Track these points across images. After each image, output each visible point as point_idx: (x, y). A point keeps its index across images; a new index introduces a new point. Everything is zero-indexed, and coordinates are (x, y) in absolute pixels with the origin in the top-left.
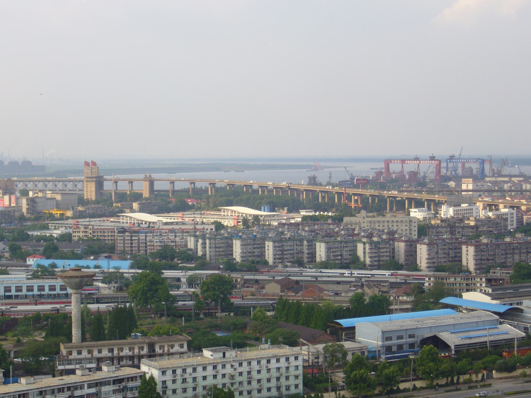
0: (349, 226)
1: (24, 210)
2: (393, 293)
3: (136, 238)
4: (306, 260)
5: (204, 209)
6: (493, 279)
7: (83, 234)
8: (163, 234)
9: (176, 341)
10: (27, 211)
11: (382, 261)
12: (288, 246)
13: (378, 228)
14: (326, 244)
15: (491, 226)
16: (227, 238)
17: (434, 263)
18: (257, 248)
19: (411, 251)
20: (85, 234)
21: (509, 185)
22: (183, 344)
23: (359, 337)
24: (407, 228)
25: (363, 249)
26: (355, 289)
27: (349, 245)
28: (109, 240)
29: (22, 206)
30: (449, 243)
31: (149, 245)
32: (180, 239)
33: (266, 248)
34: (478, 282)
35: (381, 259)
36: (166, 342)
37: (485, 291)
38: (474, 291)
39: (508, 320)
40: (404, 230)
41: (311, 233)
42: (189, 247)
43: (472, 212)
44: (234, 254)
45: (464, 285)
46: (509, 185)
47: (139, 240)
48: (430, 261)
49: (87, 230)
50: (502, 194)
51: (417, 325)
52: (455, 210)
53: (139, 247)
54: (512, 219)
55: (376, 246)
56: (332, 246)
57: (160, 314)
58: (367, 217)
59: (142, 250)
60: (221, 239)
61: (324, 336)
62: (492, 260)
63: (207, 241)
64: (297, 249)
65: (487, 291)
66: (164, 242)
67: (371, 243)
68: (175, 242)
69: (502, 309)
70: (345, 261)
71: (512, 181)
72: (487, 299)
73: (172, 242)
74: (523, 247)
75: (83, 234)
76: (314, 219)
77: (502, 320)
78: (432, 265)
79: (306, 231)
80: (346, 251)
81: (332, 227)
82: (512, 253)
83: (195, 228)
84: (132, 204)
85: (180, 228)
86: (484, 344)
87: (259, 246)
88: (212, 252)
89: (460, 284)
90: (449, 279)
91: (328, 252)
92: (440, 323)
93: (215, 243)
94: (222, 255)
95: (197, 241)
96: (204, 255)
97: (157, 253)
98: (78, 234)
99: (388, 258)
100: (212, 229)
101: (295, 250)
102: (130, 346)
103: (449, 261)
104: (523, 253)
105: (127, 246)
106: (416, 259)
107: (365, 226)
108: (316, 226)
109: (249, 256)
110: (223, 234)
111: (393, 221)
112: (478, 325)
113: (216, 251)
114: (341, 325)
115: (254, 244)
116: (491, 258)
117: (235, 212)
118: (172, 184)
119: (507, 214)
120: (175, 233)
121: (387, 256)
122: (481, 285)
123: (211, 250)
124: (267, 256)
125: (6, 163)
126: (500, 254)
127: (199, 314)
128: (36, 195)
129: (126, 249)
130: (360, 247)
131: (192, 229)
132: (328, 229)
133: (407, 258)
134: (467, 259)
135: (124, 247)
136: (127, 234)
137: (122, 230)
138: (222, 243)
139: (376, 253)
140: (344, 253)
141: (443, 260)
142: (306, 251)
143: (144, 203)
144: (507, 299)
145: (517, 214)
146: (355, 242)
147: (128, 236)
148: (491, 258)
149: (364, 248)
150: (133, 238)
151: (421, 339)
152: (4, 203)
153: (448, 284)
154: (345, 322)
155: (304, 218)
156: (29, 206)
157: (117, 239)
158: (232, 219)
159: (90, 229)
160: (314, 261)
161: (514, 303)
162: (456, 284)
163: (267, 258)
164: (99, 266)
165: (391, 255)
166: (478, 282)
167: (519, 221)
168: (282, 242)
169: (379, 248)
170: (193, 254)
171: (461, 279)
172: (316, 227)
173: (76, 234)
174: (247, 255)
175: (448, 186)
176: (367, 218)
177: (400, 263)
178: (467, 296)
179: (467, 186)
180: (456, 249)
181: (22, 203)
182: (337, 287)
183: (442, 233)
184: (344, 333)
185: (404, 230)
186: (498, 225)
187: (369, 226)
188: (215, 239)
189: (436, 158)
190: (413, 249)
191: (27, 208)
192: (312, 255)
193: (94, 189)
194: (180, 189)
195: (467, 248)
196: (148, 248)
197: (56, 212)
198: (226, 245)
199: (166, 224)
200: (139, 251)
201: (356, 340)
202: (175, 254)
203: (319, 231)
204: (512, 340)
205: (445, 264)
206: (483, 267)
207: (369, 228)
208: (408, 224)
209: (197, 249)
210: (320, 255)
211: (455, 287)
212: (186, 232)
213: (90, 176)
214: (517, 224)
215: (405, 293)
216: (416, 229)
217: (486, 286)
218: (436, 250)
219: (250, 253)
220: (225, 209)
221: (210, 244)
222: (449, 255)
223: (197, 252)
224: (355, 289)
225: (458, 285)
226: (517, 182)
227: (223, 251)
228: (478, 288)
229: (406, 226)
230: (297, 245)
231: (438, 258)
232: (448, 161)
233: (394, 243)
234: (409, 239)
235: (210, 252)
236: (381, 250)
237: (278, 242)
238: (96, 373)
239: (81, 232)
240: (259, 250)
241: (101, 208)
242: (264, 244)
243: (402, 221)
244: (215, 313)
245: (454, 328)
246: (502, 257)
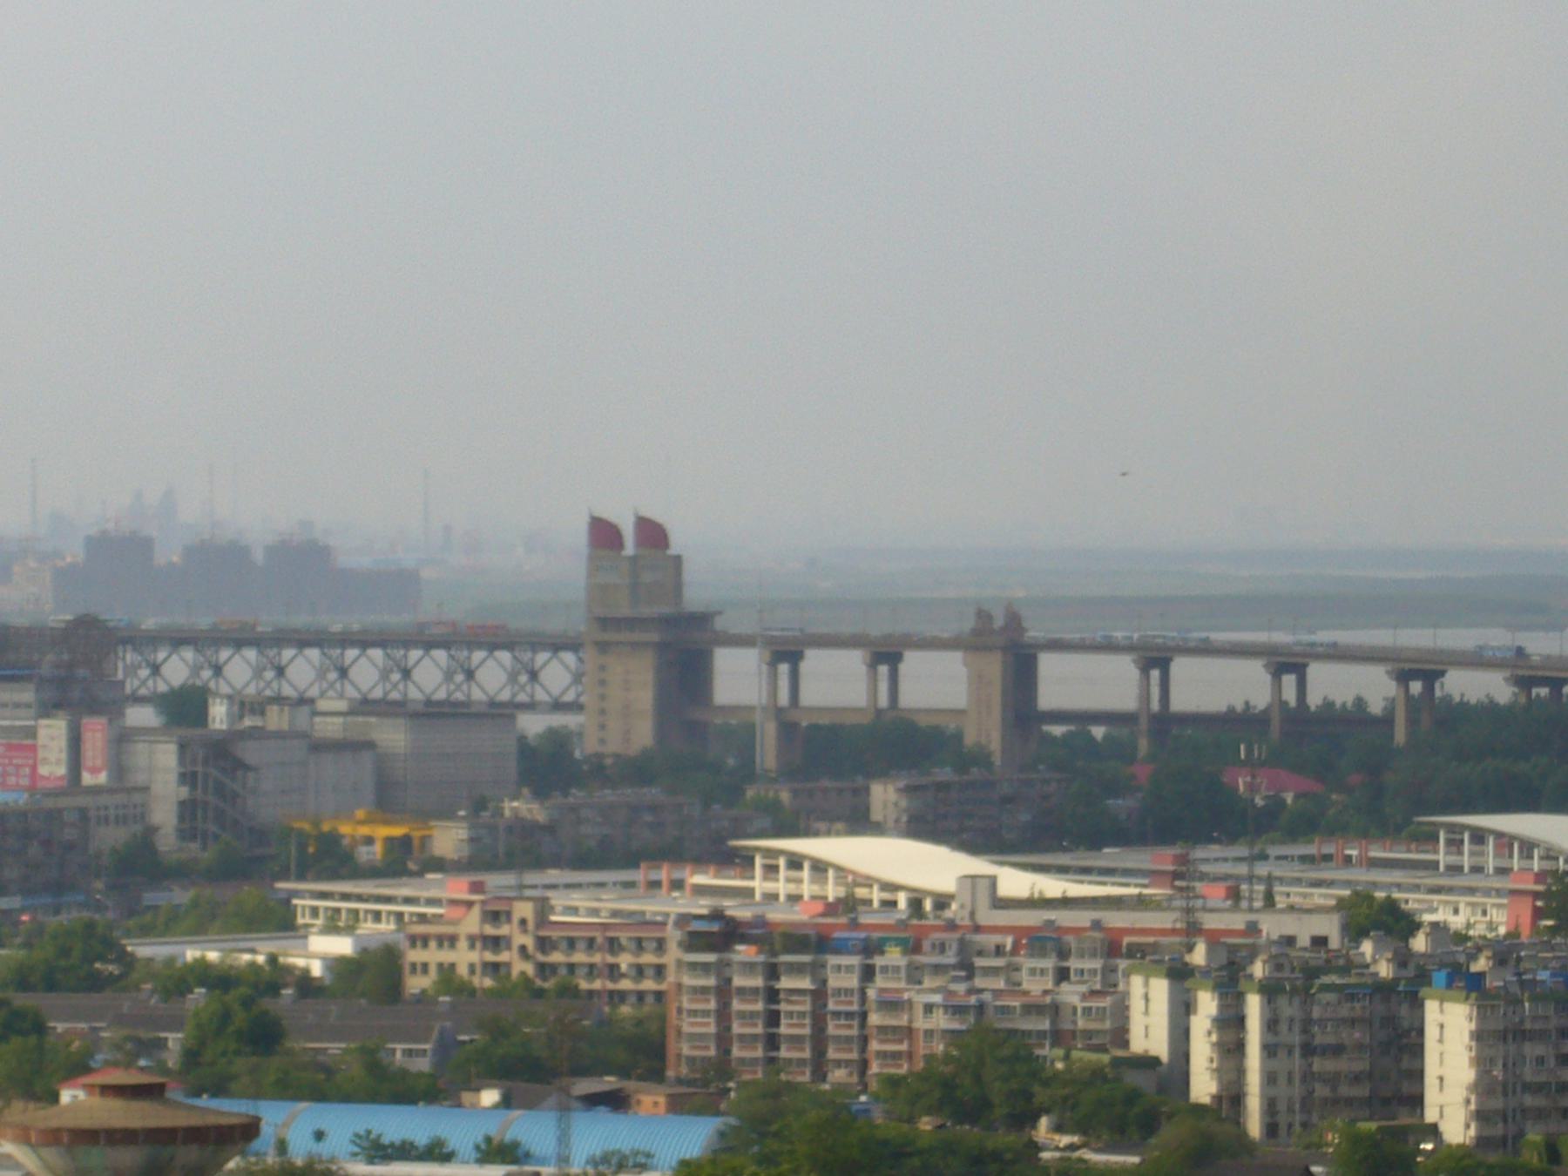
1: (164, 815)
3: (805, 983)
5: (1337, 830)
7: (475, 956)
8: (980, 962)
10: (181, 818)
16: (1384, 989)
20: (490, 957)
28: (641, 996)
29: (145, 789)
31: (882, 1029)
32: (1084, 997)
47: (819, 995)
49: (504, 930)
53: (819, 1040)
59: (838, 1063)
60: (1348, 994)
63: (1254, 1005)
68: (1055, 1010)
73: (1032, 1009)
75: (475, 956)
84: (867, 790)
88: (1282, 1080)
94: (1349, 1102)
97: (924, 1077)
98: (446, 956)
105: (742, 1037)
113: (1308, 1076)
118: (1155, 674)
120: (1063, 954)
125: (169, 553)
128: (248, 722)
129: (736, 1052)
131: (1174, 931)
135: (724, 1039)
136: (744, 952)
137: (715, 927)
138: (1352, 1022)
143: (942, 787)
147: (749, 967)
150: (785, 983)
152: (34, 768)
156: (193, 786)
157: (679, 986)
158: (1499, 892)
159: (523, 922)
164: (515, 1145)
173: (433, 955)
191: (182, 804)
193: (644, 698)
196: (874, 1046)
197: (364, 830)
200: (819, 1067)
202: (1036, 1088)
213: (625, 611)
219: (1537, 1088)
220: (1464, 827)
221: (1271, 1025)
227: (1356, 1079)
239: (463, 944)
241: (653, 808)
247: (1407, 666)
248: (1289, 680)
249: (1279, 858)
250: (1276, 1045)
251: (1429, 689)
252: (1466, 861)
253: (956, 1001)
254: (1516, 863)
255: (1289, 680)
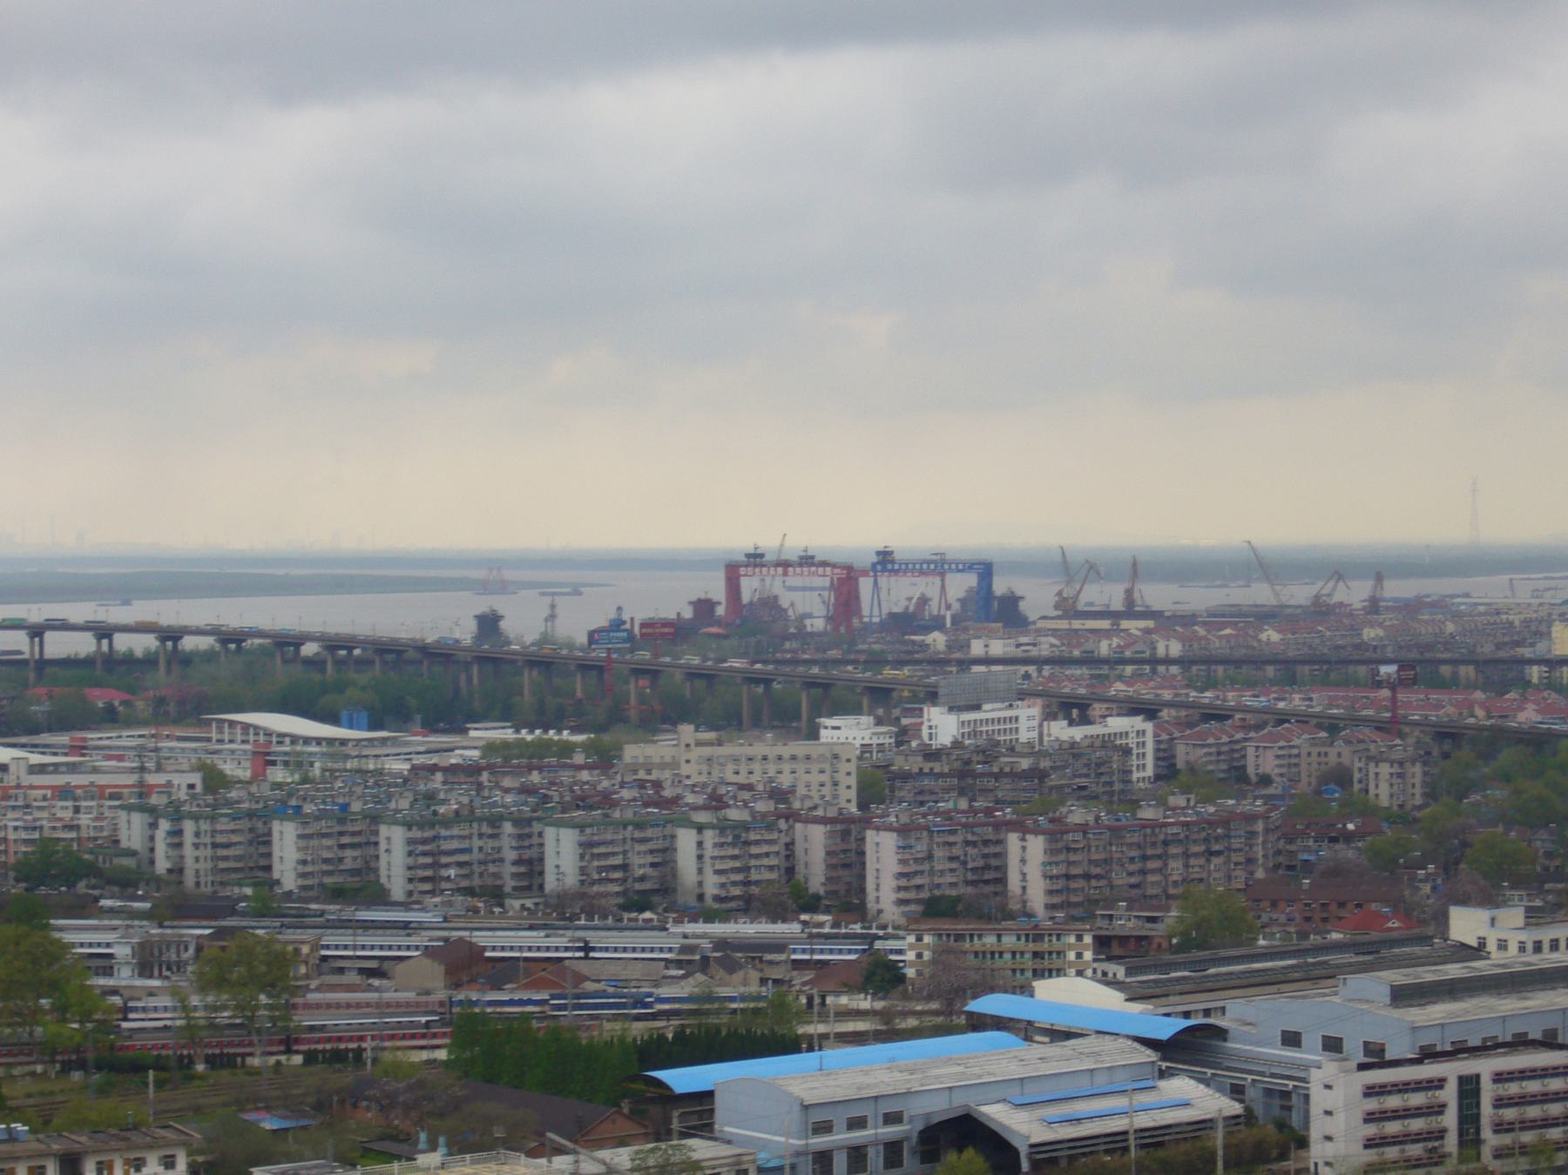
0: (642, 775)
2: (804, 984)
4: (509, 884)
6: (1115, 936)
9: (150, 1147)
11: (757, 883)
12: (452, 837)
13: (731, 778)
14: (577, 831)
15: (1080, 772)
16: (251, 815)
17: (919, 887)
18: (353, 846)
19: (845, 851)
21: (1115, 642)
22: (173, 1156)
23: (725, 1124)
24: (824, 778)
25: (694, 845)
26: (682, 972)
27: (649, 833)
30: (965, 826)
33: (383, 846)
34: (1070, 947)
35: (754, 876)
36: (118, 1150)
37: (1105, 974)
38: (1058, 976)
39: (1184, 1063)
40: (815, 787)
41: (522, 797)
42: (124, 844)
43: (1017, 729)
44: (277, 867)
45: (1028, 956)
46: (1115, 642)
48: (903, 882)
50: (1093, 672)
51: (908, 1081)
52: (963, 722)
54: (1141, 751)
55: (737, 837)
56: (596, 838)
57: (63, 1062)
58: (699, 744)
61: (614, 1122)
62: (1098, 877)
63: (189, 827)
64: (481, 849)
65: (1110, 975)
66: (41, 828)
67: (722, 827)
68: (78, 828)
69: (1165, 1028)
70: (638, 886)
71: (1123, 630)
72: (1111, 999)
74: (1195, 836)
76: (535, 755)
77: (1164, 1065)
78: (911, 895)
79: (507, 791)
80: (639, 853)
81: (585, 775)
82: (1159, 857)
83: (141, 784)
85: (92, 784)
86: (1118, 1138)
87: (356, 840)
89: (1014, 953)
90: (1058, 939)
91: (582, 857)
92: (980, 1077)
93: (214, 832)
95: (154, 826)
96: (177, 871)
99: (773, 876)
100: (191, 786)
101: (476, 850)
102: (99, 1159)
103: (968, 883)
104: (1196, 855)
106: (862, 877)
107: (694, 772)
108: (535, 773)
109: (325, 873)
110: (238, 802)
111: (780, 758)
112: (1095, 1084)
113: (215, 858)
114: (667, 1087)
115: (341, 834)
116: (1096, 871)
117: (256, 728)
118: (37, 639)
119: (1127, 733)
121: (771, 868)
122: (1079, 955)
123: (197, 853)
124: (383, 872)
126: (1124, 860)
127: (192, 1062)
130: (686, 840)
132: (575, 783)
133: (834, 874)
134: (1024, 875)
138: (233, 831)
139: (734, 857)
140: (635, 860)
141: (949, 879)
142: (510, 855)
144: (1178, 999)
145: (1156, 735)
146: (669, 825)
148: (1098, 870)
149: (700, 844)
151: (921, 1128)
153: (976, 954)
154: (681, 1079)
155: (490, 748)
160: (535, 887)
161: (1196, 1011)
162: (1001, 954)
163: (383, 880)
165: (784, 864)
166: (1070, 947)
167: (1161, 754)
168: (432, 826)
169: (747, 843)
170: (139, 866)
171: (1019, 939)
172: (535, 777)
174: (317, 868)
175: (924, 646)
176: (700, 749)
177: (811, 891)
178: (1047, 989)
179: (986, 646)
180: (986, 843)
181: (1531, 674)
182: (625, 969)
183: (932, 793)
184: (676, 1114)
185: (815, 787)
186: (1102, 770)
187: (705, 774)
188: (213, 818)
189: (816, 560)
190: (853, 846)
192: (532, 868)
194: (65, 656)
195: (1023, 839)
198: (249, 836)
199: (41, 769)
201: (717, 1134)
203: (549, 789)
204: (1209, 1125)
205: (954, 893)
206: (1074, 899)
207: (703, 779)
208: (827, 767)
209: (152, 850)
210: (557, 867)
211: (999, 963)
212: (112, 797)
214: (1156, 766)
215: (845, 985)
216: (853, 781)
217: (1095, 960)
218: (925, 848)
219: (326, 861)
221: (197, 834)
222: (965, 863)
223: (152, 862)
224: (682, 972)
225: (1007, 956)
226: (1138, 633)
227: (238, 858)
228: (1071, 965)
229: (822, 772)
230: (481, 836)
231: (932, 872)
232: (879, 567)
233: (791, 827)
234: (841, 814)
235: (197, 859)
236: (754, 850)
237: (421, 827)
238: (1334, 1157)
240: (356, 853)
242: (377, 833)
243: (808, 758)
244: (244, 1055)
245: (1021, 1092)
246: (1132, 868)
247: (165, 634)
248: (105, 642)
249: (128, 736)
250: (199, 844)
251: (175, 646)
252: (227, 737)
253: (28, 825)
254: (252, 738)
255: (105, 642)
